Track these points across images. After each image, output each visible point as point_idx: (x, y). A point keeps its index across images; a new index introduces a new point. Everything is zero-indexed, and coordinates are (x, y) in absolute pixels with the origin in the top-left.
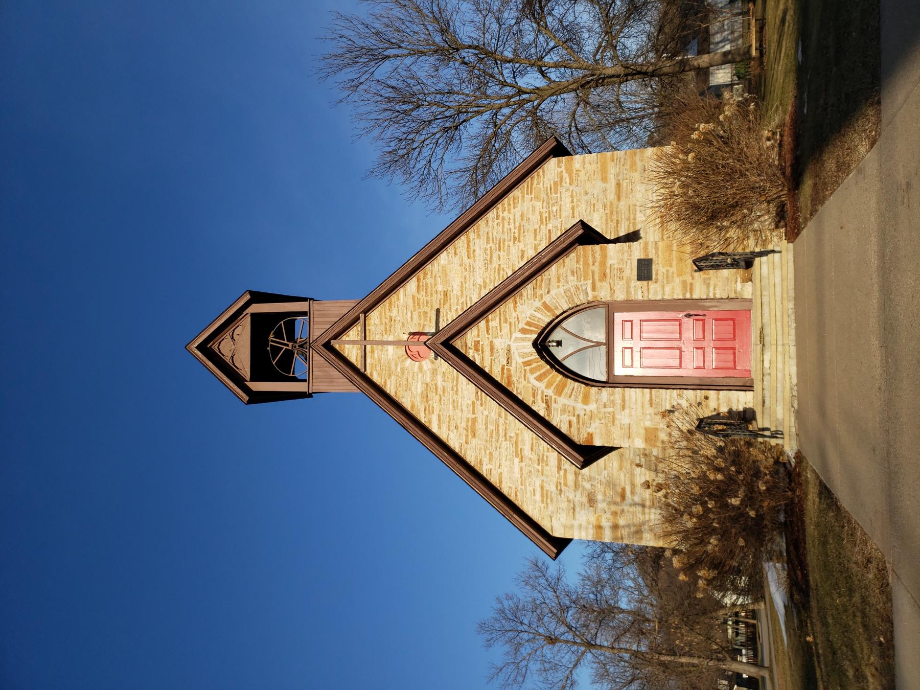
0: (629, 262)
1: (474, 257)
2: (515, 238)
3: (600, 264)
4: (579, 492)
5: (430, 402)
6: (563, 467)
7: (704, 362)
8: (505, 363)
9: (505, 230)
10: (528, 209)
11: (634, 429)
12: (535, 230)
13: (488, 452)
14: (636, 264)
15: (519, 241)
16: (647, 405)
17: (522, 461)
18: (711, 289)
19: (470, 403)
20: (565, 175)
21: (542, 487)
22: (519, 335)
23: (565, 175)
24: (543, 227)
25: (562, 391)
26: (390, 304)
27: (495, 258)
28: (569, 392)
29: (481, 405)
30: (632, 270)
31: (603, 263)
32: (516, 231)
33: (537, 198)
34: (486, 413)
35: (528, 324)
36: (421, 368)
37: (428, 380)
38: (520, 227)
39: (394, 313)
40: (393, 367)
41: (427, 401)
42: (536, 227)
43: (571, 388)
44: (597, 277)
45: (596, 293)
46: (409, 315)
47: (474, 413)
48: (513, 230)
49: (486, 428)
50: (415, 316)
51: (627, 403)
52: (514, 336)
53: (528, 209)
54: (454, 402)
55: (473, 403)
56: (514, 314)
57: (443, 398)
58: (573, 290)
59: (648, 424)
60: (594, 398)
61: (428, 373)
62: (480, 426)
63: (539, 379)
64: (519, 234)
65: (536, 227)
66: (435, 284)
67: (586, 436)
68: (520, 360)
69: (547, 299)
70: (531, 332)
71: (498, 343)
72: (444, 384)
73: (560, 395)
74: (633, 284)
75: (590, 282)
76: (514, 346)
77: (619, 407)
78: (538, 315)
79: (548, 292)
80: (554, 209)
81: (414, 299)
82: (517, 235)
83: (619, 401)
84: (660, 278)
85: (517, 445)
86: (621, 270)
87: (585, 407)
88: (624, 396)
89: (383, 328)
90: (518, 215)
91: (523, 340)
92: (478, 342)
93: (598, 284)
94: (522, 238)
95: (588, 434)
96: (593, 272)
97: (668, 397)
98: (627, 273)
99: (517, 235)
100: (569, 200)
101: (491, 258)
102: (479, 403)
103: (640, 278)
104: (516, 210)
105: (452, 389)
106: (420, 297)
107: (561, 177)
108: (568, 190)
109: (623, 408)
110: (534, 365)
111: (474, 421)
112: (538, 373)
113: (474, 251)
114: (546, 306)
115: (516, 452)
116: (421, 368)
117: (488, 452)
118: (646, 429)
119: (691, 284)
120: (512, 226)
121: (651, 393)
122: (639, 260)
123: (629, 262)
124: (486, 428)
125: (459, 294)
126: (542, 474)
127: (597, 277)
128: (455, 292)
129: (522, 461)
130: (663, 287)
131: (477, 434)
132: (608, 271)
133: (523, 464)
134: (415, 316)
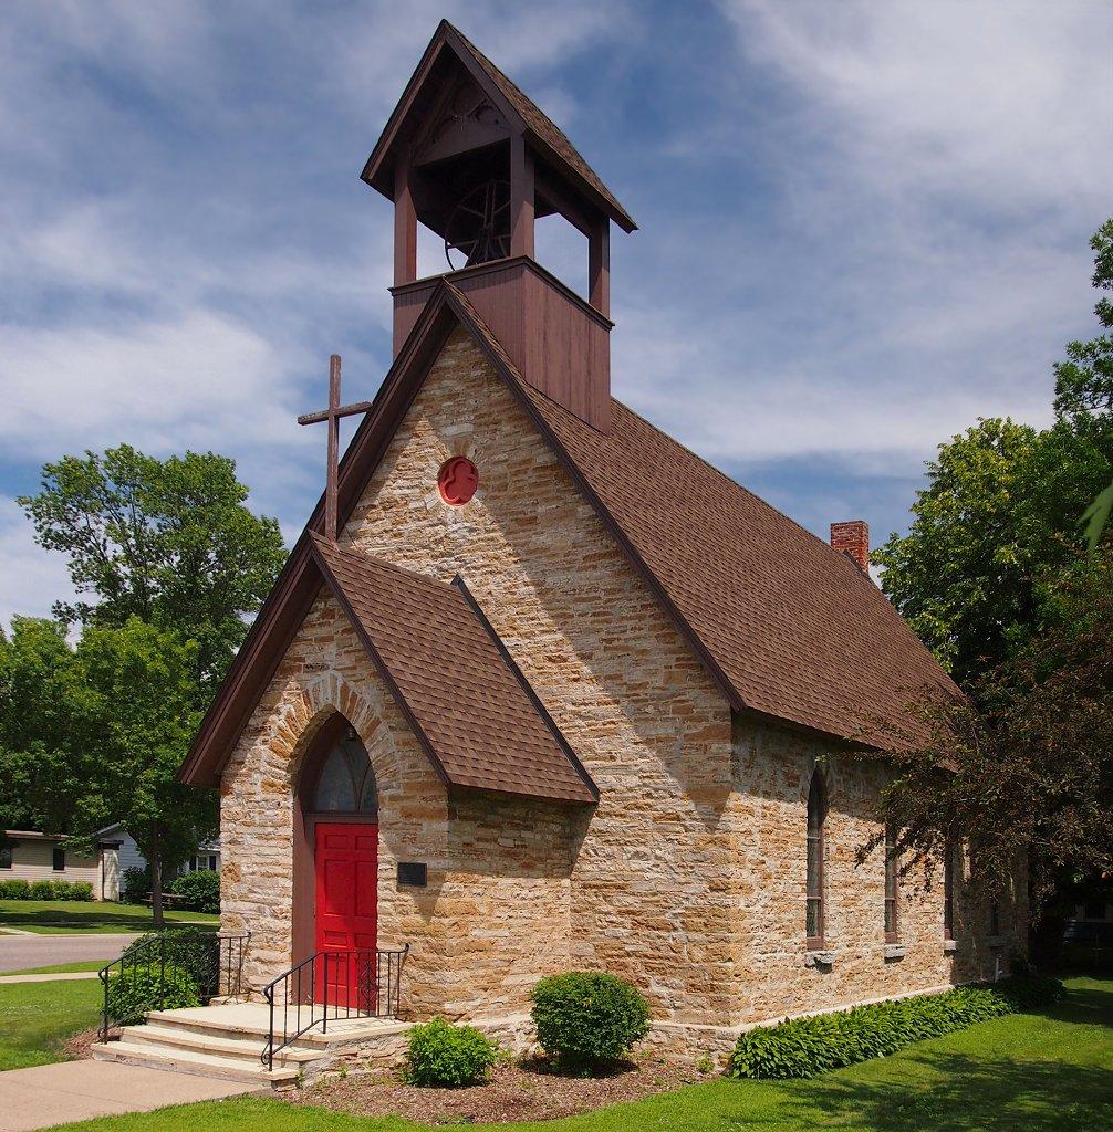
0: (423, 852)
1: (586, 569)
2: (613, 640)
3: (423, 809)
8: (308, 662)
9: (625, 623)
10: (654, 662)
12: (619, 677)
14: (420, 861)
15: (606, 649)
20: (701, 727)
23: (701, 727)
24: (624, 690)
27: (582, 606)
30: (415, 854)
31: (423, 814)
32: (621, 643)
33: (669, 678)
35: (354, 696)
38: (628, 648)
39: (506, 428)
42: (626, 679)
48: (622, 636)
50: (501, 469)
52: (338, 674)
53: (654, 662)
56: (365, 674)
58: (393, 767)
64: (616, 648)
65: (626, 679)
66: (546, 500)
70: (343, 703)
71: (331, 648)
75: (401, 792)
76: (326, 675)
80: (650, 709)
81: (524, 462)
82: (615, 644)
89: (485, 410)
90: (646, 645)
91: (334, 690)
93: (397, 805)
94: (609, 653)
96: (413, 797)
98: (412, 850)
99: (615, 644)
100: (661, 732)
101: (584, 600)
103: (560, 858)
104: (653, 640)
106: (530, 473)
107: (700, 720)
108: (678, 731)
113: (595, 567)
120: (629, 634)
122: (423, 866)
123: (423, 852)
125: (532, 547)
128: (534, 538)
132: (414, 820)
134: (501, 469)
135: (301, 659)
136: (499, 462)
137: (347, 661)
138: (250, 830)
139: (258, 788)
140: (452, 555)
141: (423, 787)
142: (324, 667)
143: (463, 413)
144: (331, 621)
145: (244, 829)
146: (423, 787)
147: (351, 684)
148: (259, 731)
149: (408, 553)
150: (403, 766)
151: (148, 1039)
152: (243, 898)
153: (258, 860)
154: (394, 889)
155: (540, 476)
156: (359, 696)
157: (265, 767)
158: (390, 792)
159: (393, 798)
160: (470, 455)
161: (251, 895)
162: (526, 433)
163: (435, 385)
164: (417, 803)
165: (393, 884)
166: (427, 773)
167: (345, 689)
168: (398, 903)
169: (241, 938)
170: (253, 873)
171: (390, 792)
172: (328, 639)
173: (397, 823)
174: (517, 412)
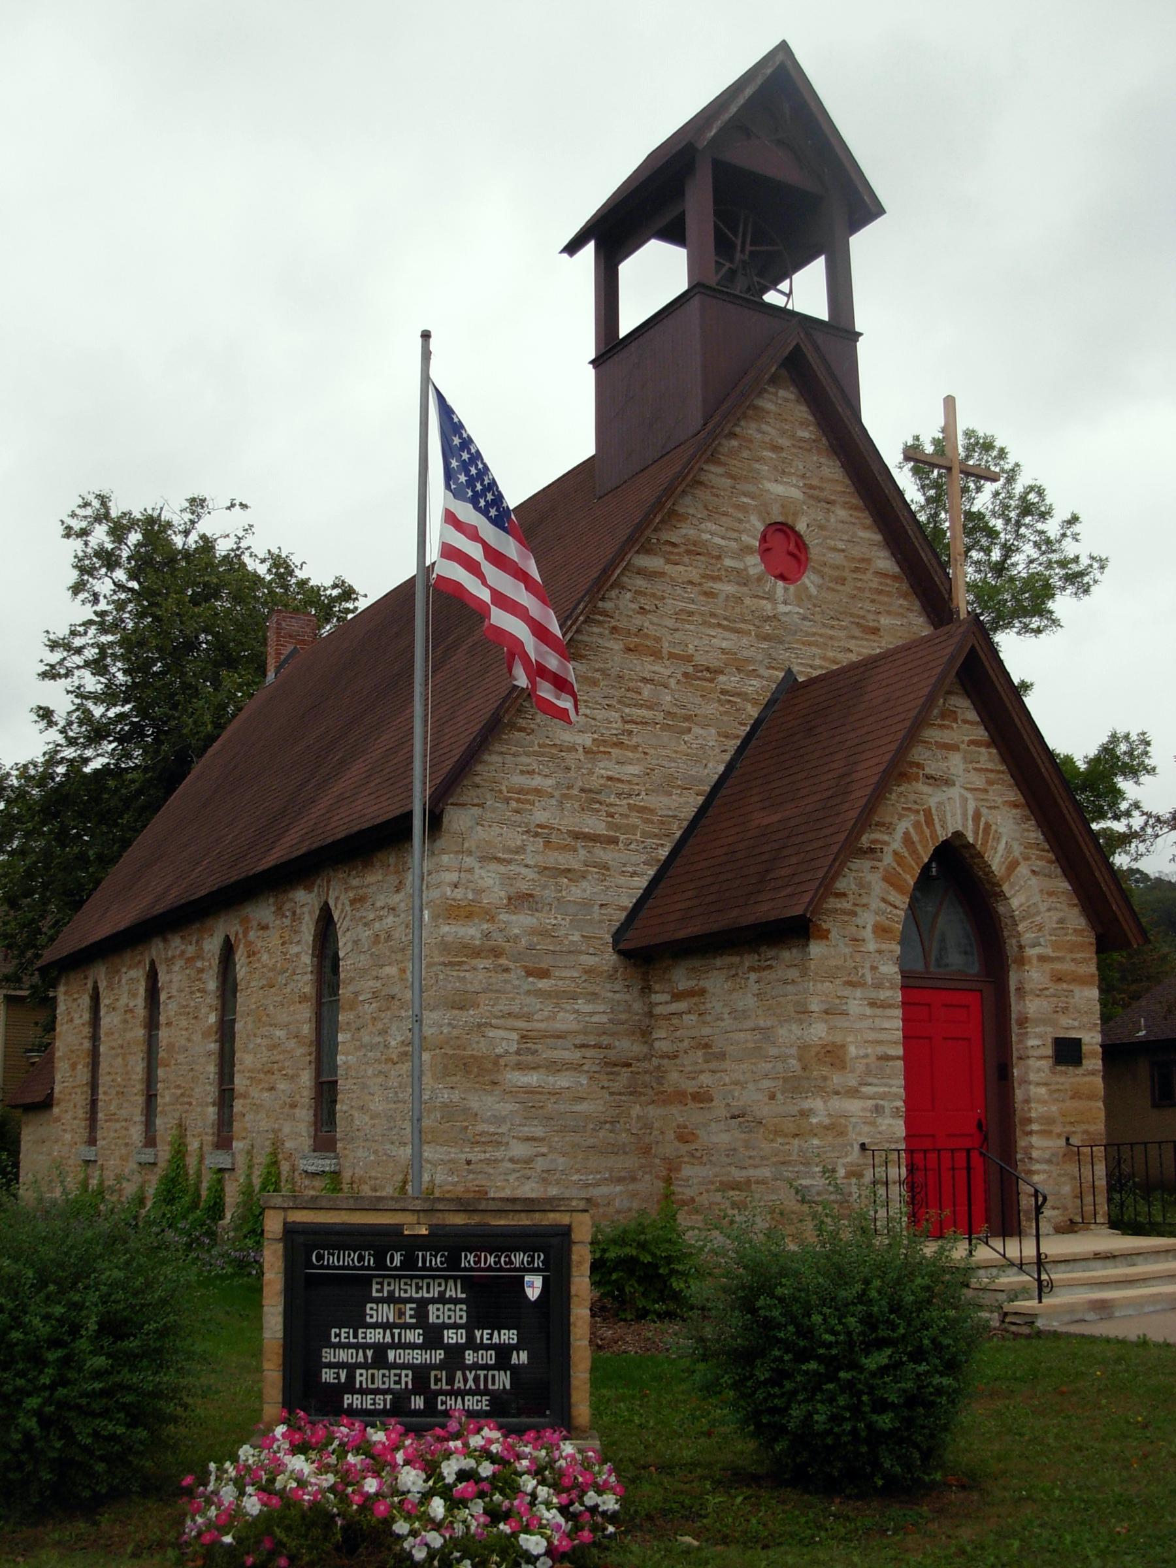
4: (536, 876)
5: (686, 559)
6: (580, 844)
7: (953, 1158)
8: (928, 771)
11: (840, 1022)
13: (597, 675)
14: (1074, 1035)
16: (880, 1050)
17: (587, 751)
18: (1045, 1167)
19: (691, 649)
21: (537, 791)
22: (971, 806)
25: (892, 884)
26: (856, 508)
28: (891, 899)
29: (685, 675)
34: (672, 682)
35: (988, 826)
36: (747, 550)
37: (728, 562)
39: (842, 513)
40: (750, 488)
41: (688, 552)
43: (897, 903)
44: (1058, 966)
45: (1035, 962)
46: (841, 545)
47: (671, 656)
49: (645, 680)
50: (838, 559)
51: (878, 1011)
54: (691, 614)
55: (689, 659)
56: (1000, 800)
57: (697, 589)
59: (852, 1050)
60: (884, 947)
61: (738, 565)
62: (648, 667)
63: (907, 840)
66: (889, 613)
67: (825, 926)
68: (932, 802)
69: (1023, 870)
72: (722, 597)
73: (885, 879)
74: (1050, 1029)
75: (1049, 951)
77: (873, 995)
78: (1001, 847)
79: (1033, 872)
83: (884, 994)
84: (1058, 1079)
85: (615, 745)
86: (1065, 1010)
87: (869, 928)
88: (890, 1006)
91: (965, 815)
92: (955, 720)
93: (1047, 967)
95: (828, 931)
97: (894, 1090)
98: (1065, 1021)
102: (690, 670)
105: (713, 615)
109: (872, 1004)
110: (927, 832)
111: (656, 654)
112: (916, 838)
114: (1013, 866)
115: (605, 742)
116: (747, 550)
117: (597, 675)
118: (843, 1046)
119: (1050, 1132)
121: (898, 1058)
122: (1080, 1040)
123: (1076, 1024)
124: (645, 680)
126: (564, 796)
127: (1058, 966)
129: (587, 751)
130: (1045, 1084)
131: (631, 656)
132: (1065, 986)
133: (580, 754)
135: (919, 766)
136: (834, 549)
137: (979, 781)
138: (859, 993)
139: (868, 933)
140: (782, 642)
141: (1073, 947)
142: (948, 783)
143: (790, 474)
144: (955, 725)
145: (848, 991)
146: (1073, 947)
147: (984, 811)
148: (871, 852)
149: (725, 623)
150: (1050, 919)
151: (1114, 1257)
152: (853, 1093)
153: (872, 1036)
154: (1047, 1070)
155: (881, 584)
156: (994, 827)
157: (875, 904)
158: (1037, 950)
159: (1042, 958)
160: (801, 527)
161: (864, 1089)
162: (865, 528)
163: (754, 425)
164: (1066, 967)
165: (1045, 1064)
166: (1075, 930)
167: (977, 816)
168: (1053, 1087)
169: (925, 1152)
170: (866, 1056)
171: (1037, 950)
172: (954, 748)
173: (1047, 989)
174: (854, 501)
